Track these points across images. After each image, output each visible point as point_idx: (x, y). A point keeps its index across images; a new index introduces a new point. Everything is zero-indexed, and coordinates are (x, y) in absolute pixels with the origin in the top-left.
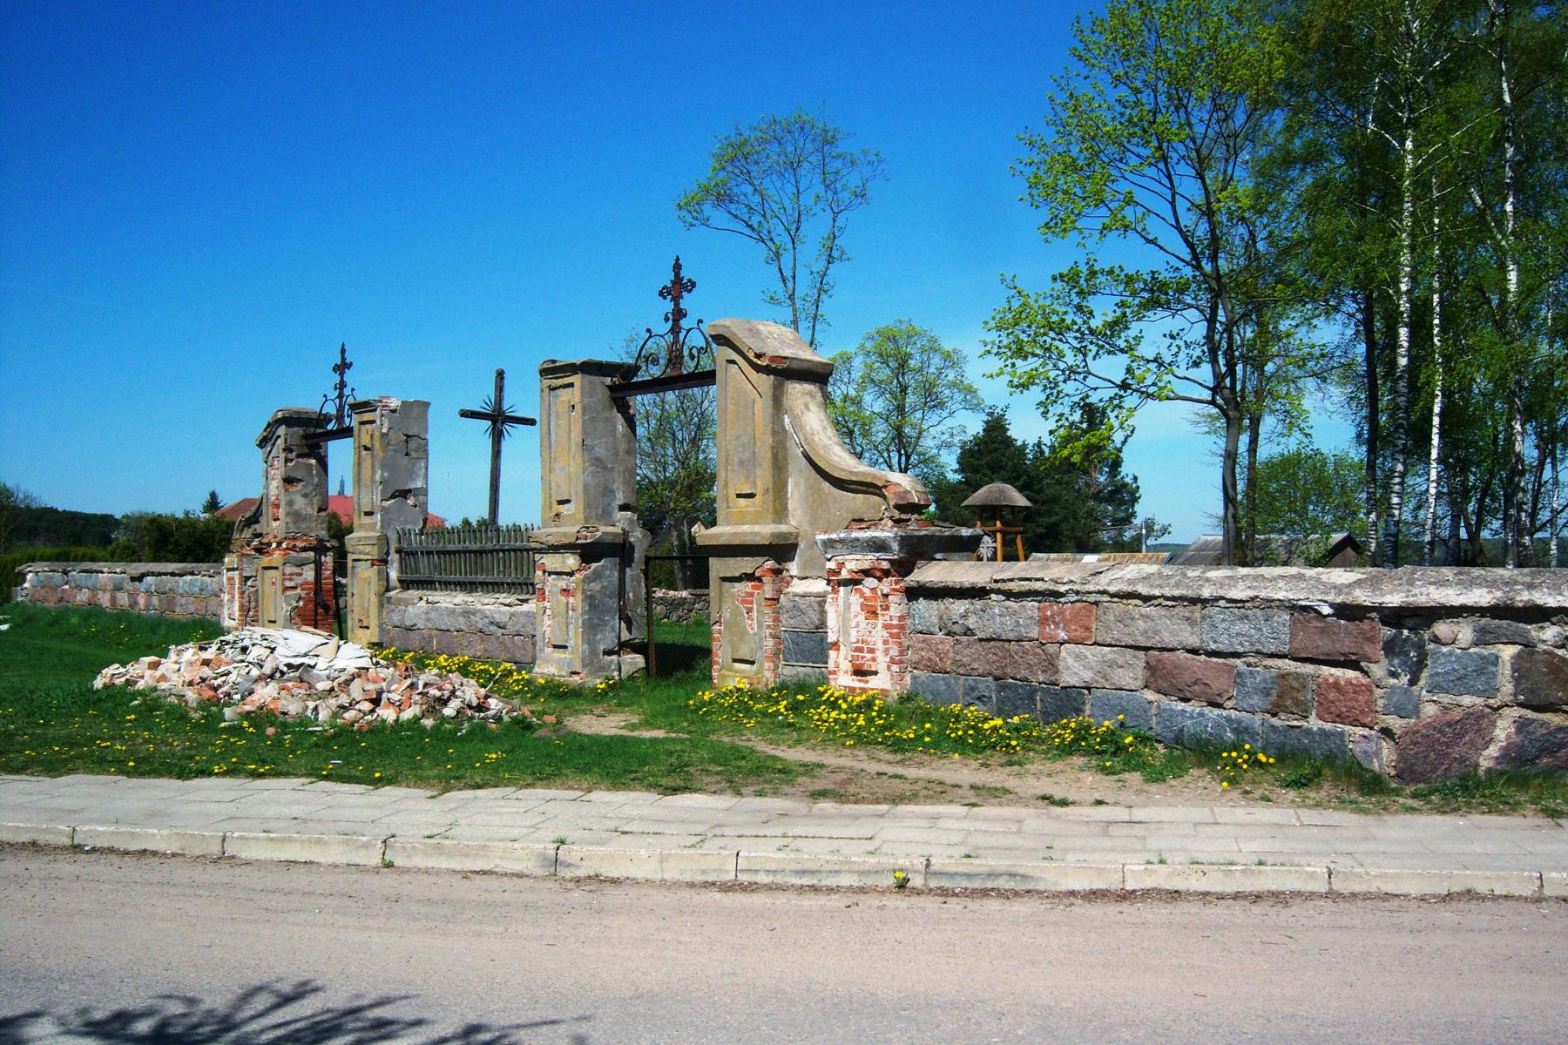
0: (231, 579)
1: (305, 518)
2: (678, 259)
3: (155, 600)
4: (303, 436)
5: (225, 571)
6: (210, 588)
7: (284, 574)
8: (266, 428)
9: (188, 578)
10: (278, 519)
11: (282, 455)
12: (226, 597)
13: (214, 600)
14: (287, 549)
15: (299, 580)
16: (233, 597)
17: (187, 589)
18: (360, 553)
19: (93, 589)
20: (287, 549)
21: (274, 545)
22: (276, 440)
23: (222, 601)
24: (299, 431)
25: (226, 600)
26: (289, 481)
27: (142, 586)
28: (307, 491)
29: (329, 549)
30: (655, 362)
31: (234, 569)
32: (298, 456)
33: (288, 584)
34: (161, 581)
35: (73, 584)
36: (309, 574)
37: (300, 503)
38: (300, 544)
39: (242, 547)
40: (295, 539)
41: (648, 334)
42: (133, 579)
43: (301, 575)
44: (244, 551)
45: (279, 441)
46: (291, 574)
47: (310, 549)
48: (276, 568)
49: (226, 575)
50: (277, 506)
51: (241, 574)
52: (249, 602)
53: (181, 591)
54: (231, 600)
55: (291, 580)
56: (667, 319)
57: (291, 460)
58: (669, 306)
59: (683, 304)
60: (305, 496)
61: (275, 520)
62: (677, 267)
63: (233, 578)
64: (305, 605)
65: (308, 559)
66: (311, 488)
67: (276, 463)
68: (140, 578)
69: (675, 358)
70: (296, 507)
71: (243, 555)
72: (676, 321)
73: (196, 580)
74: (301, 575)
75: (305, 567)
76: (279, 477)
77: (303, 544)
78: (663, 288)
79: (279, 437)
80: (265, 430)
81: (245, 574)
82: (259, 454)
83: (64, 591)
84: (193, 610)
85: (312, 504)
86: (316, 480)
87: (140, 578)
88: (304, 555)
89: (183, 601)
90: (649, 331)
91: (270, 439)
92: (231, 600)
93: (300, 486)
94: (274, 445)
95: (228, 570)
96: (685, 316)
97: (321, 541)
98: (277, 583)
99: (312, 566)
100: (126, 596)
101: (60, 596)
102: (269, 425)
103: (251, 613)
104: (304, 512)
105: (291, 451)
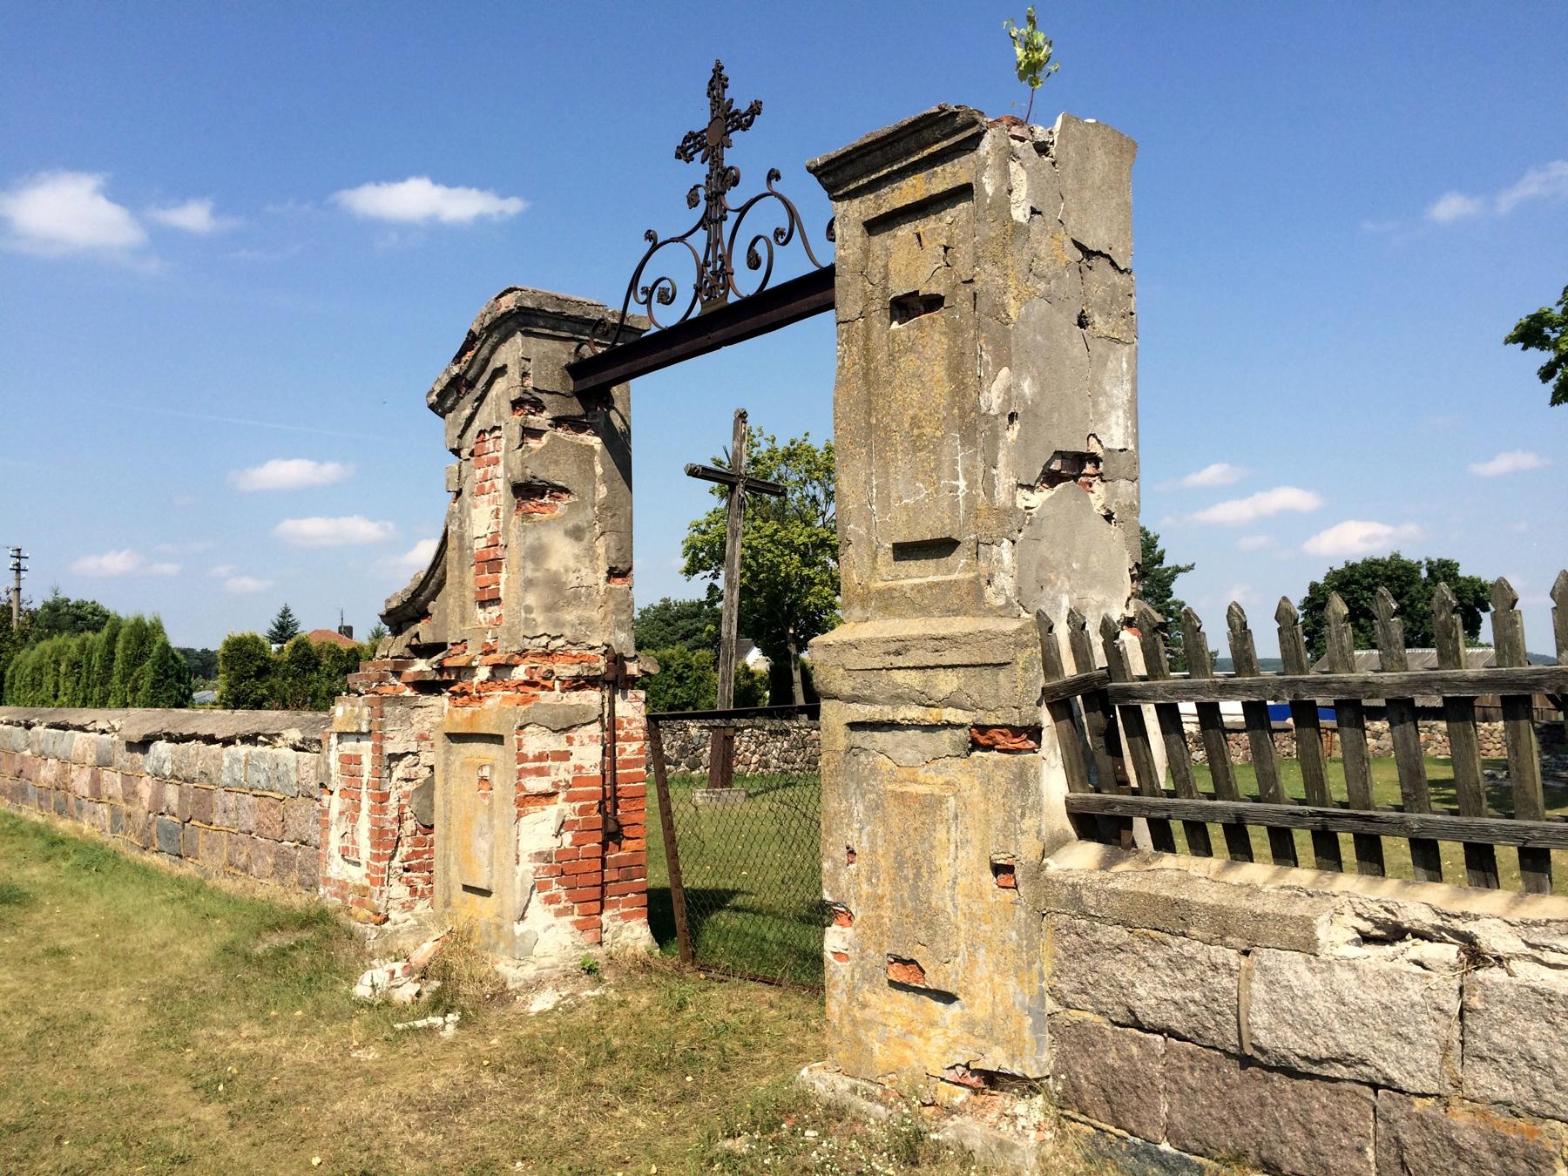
0: (351, 761)
1: (577, 597)
2: (718, 69)
3: (171, 794)
4: (570, 368)
5: (334, 739)
6: (294, 779)
7: (522, 758)
8: (462, 353)
9: (241, 750)
10: (496, 601)
11: (514, 421)
12: (335, 804)
13: (303, 808)
14: (531, 683)
15: (562, 772)
16: (358, 808)
17: (239, 775)
18: (898, 699)
19: (64, 761)
20: (531, 683)
21: (483, 673)
22: (489, 384)
23: (325, 813)
24: (564, 353)
25: (334, 813)
26: (526, 490)
27: (147, 762)
28: (581, 519)
29: (632, 682)
30: (667, 299)
31: (359, 735)
32: (558, 422)
33: (535, 784)
34: (185, 753)
35: (36, 749)
36: (588, 753)
37: (563, 553)
38: (567, 670)
39: (381, 680)
40: (548, 654)
41: (649, 244)
42: (131, 746)
43: (565, 756)
44: (387, 690)
45: (500, 385)
46: (541, 757)
47: (591, 682)
48: (497, 739)
49: (335, 752)
50: (494, 564)
51: (378, 749)
52: (400, 819)
53: (226, 779)
54: (352, 813)
55: (540, 772)
56: (692, 201)
57: (537, 434)
58: (698, 171)
59: (729, 158)
60: (576, 534)
61: (483, 604)
62: (718, 81)
63: (357, 760)
64: (577, 843)
65: (586, 710)
66: (591, 513)
67: (490, 445)
68: (144, 745)
69: (713, 277)
70: (553, 565)
71: (383, 700)
72: (715, 198)
73: (261, 756)
74: (565, 756)
75: (578, 734)
76: (500, 484)
77: (574, 670)
78: (686, 139)
79: (501, 371)
80: (458, 359)
81: (390, 748)
82: (441, 431)
83: (23, 758)
84: (251, 825)
85: (593, 558)
86: (602, 491)
87: (144, 745)
88: (574, 698)
89: (231, 800)
90: (650, 236)
91: (471, 385)
92: (352, 813)
93: (562, 506)
94: (481, 399)
95: (341, 736)
96: (735, 182)
97: (617, 660)
98: (495, 780)
99: (595, 729)
100: (118, 778)
101: (17, 767)
102: (471, 340)
103: (404, 850)
104: (572, 581)
105: (538, 407)
